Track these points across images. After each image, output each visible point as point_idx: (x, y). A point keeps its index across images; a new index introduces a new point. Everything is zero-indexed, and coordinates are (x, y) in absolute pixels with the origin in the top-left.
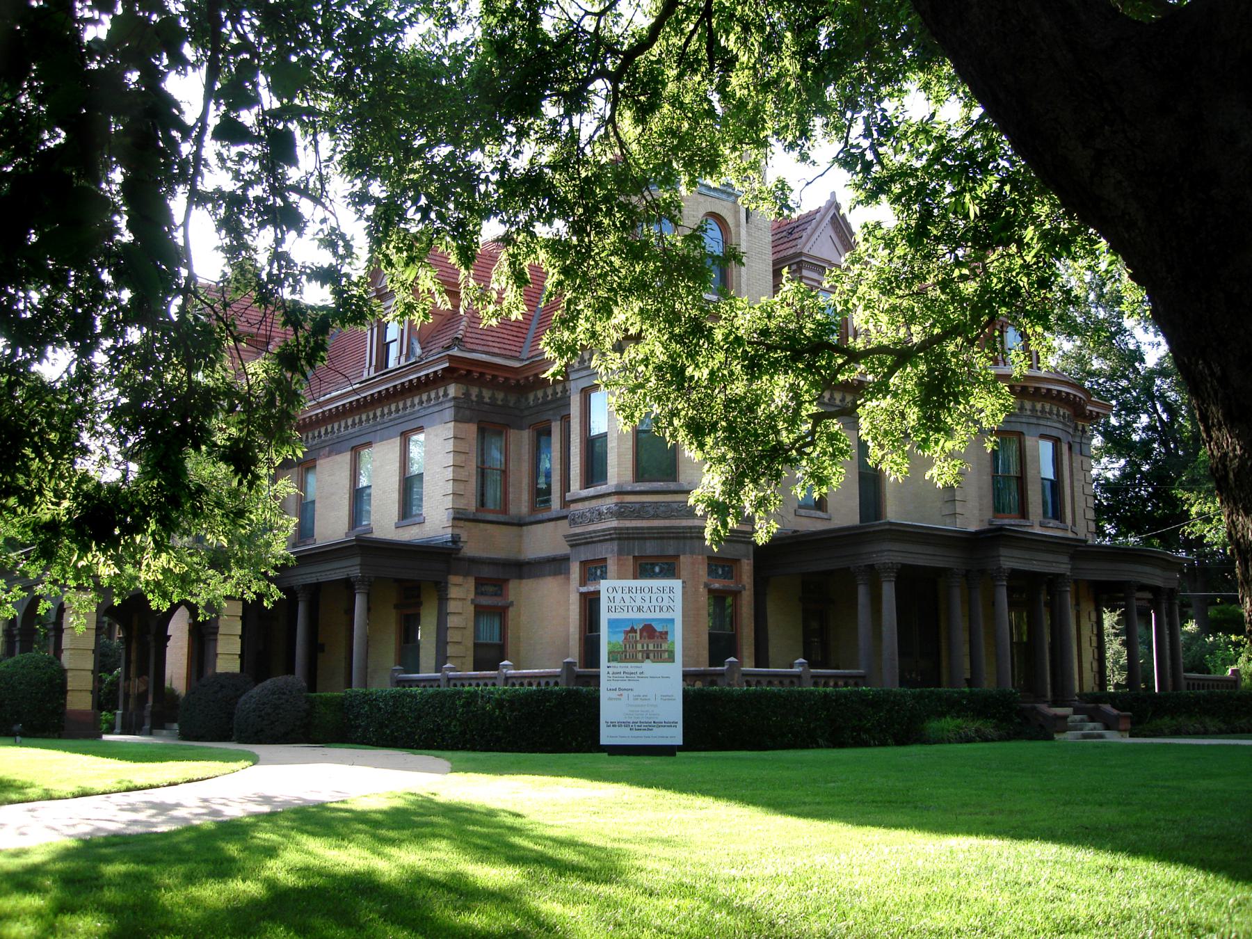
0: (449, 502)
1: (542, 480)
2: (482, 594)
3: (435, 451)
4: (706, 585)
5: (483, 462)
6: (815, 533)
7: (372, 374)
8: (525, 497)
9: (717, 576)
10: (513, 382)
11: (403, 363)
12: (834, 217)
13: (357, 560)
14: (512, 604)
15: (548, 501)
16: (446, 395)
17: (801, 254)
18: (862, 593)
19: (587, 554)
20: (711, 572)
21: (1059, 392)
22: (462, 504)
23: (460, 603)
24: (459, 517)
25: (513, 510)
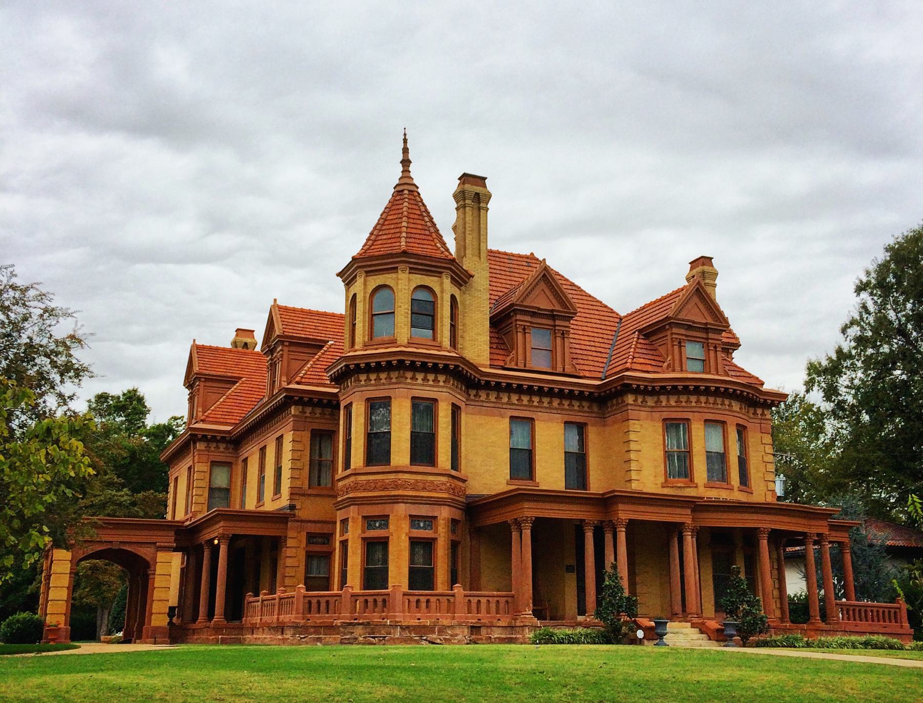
12: (544, 276)
22: (298, 483)
23: (294, 550)
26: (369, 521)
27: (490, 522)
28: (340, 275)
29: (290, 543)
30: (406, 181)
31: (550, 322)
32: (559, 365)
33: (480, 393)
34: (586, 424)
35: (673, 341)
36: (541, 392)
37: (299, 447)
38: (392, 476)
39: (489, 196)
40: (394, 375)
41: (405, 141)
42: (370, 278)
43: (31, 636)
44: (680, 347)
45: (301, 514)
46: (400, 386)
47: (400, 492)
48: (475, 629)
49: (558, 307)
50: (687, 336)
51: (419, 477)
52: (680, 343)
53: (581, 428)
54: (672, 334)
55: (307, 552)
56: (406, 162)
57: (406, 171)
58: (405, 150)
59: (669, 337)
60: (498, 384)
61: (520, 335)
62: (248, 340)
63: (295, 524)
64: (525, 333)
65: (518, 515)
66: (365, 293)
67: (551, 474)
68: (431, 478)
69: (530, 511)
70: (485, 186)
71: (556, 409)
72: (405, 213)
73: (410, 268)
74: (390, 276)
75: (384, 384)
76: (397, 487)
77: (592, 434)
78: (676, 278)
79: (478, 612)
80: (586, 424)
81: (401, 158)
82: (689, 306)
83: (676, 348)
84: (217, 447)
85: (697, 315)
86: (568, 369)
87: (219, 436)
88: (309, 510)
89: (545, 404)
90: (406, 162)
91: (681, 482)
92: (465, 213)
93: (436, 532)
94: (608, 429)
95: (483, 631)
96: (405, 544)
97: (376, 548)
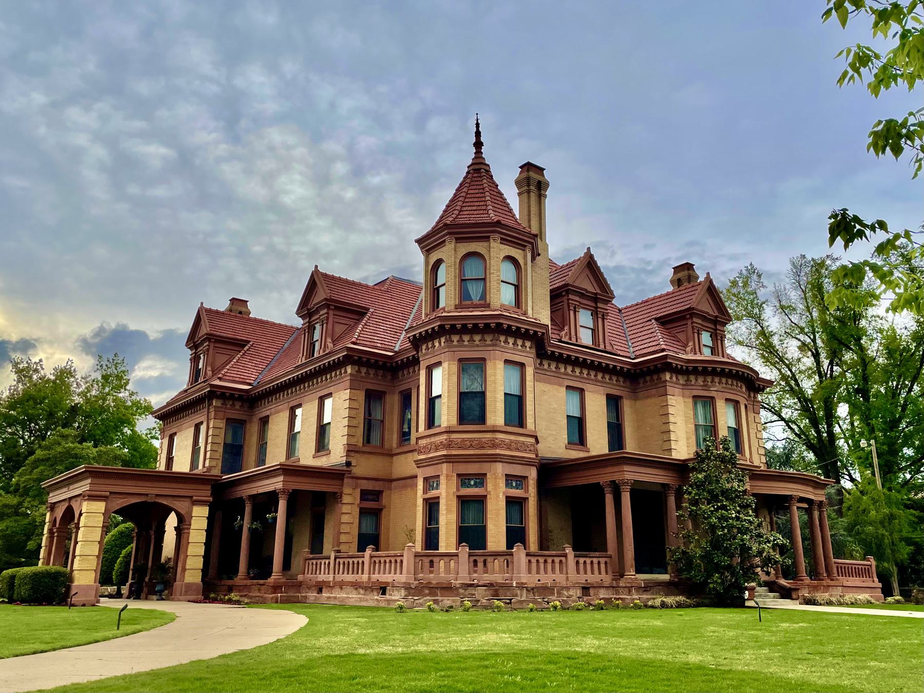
0: (344, 440)
1: (406, 426)
2: (365, 500)
3: (338, 407)
4: (504, 493)
5: (370, 415)
6: (572, 460)
7: (304, 361)
8: (395, 437)
9: (512, 487)
10: (389, 365)
11: (322, 354)
12: (589, 263)
13: (281, 478)
14: (385, 507)
15: (409, 439)
16: (346, 372)
17: (693, 309)
18: (609, 499)
19: (430, 471)
20: (508, 485)
21: (743, 373)
22: (353, 441)
23: (349, 507)
24: (351, 450)
25: (386, 446)
26: (464, 480)
27: (570, 483)
28: (419, 241)
29: (346, 499)
34: (620, 397)
37: (355, 405)
38: (489, 435)
39: (547, 185)
40: (489, 338)
42: (458, 245)
43: (53, 591)
45: (357, 471)
46: (494, 348)
47: (498, 451)
48: (586, 590)
51: (513, 438)
55: (361, 509)
56: (478, 145)
57: (478, 152)
58: (478, 134)
61: (572, 313)
62: (243, 309)
63: (350, 481)
65: (616, 477)
66: (455, 258)
67: (598, 442)
68: (522, 439)
69: (631, 474)
70: (543, 176)
72: (487, 189)
73: (502, 239)
74: (481, 244)
75: (478, 346)
76: (494, 446)
77: (627, 407)
79: (600, 574)
80: (620, 397)
83: (696, 335)
84: (233, 405)
85: (588, 286)
86: (609, 348)
87: (219, 391)
88: (365, 466)
89: (592, 377)
90: (478, 145)
92: (529, 197)
93: (527, 491)
94: (638, 403)
95: (592, 591)
96: (503, 503)
97: (471, 506)
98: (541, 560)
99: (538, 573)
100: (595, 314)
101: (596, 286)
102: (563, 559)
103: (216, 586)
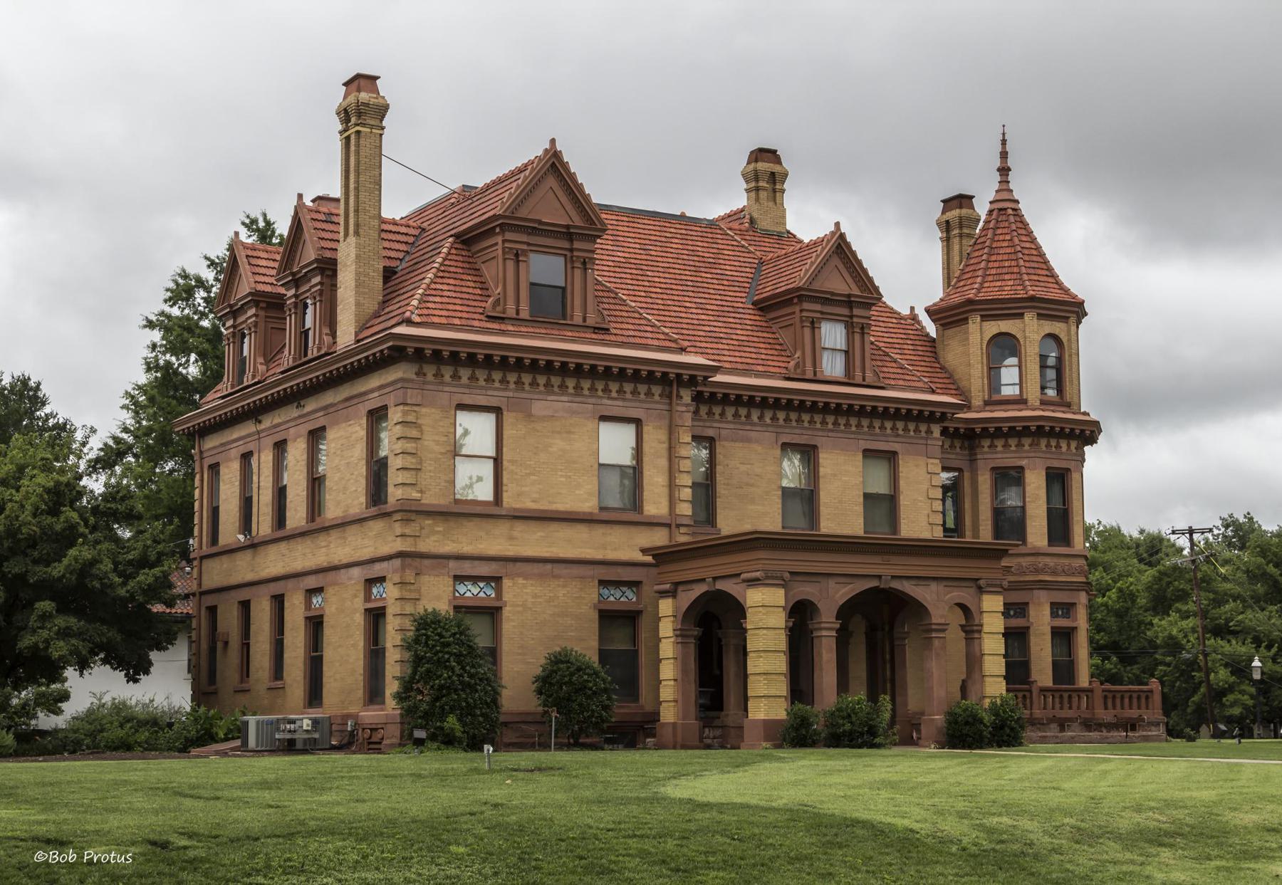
30: (1005, 195)
31: (846, 311)
32: (858, 373)
33: (443, 372)
35: (802, 321)
36: (838, 410)
41: (1004, 142)
42: (985, 324)
44: (813, 328)
49: (578, 221)
50: (529, 244)
52: (812, 323)
53: (809, 454)
54: (801, 311)
57: (1005, 182)
58: (1004, 155)
59: (500, 247)
60: (579, 366)
64: (518, 262)
71: (768, 425)
78: (832, 228)
81: (998, 164)
82: (540, 192)
83: (807, 331)
85: (839, 284)
86: (869, 381)
90: (1004, 171)
91: (709, 529)
98: (1057, 695)
99: (1114, 708)
100: (850, 327)
101: (850, 280)
102: (1027, 694)
103: (797, 735)
